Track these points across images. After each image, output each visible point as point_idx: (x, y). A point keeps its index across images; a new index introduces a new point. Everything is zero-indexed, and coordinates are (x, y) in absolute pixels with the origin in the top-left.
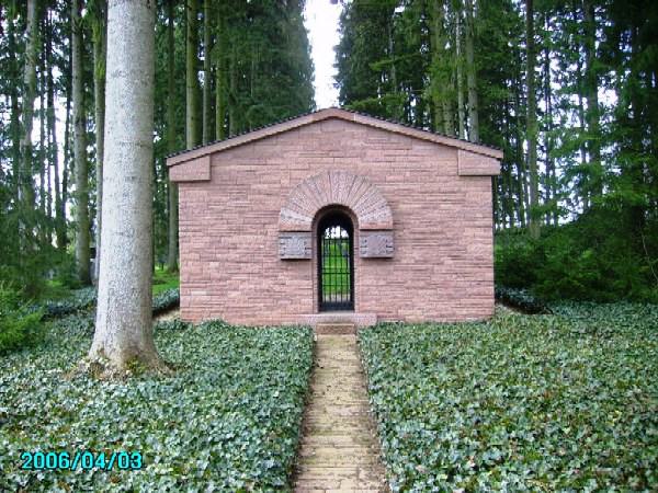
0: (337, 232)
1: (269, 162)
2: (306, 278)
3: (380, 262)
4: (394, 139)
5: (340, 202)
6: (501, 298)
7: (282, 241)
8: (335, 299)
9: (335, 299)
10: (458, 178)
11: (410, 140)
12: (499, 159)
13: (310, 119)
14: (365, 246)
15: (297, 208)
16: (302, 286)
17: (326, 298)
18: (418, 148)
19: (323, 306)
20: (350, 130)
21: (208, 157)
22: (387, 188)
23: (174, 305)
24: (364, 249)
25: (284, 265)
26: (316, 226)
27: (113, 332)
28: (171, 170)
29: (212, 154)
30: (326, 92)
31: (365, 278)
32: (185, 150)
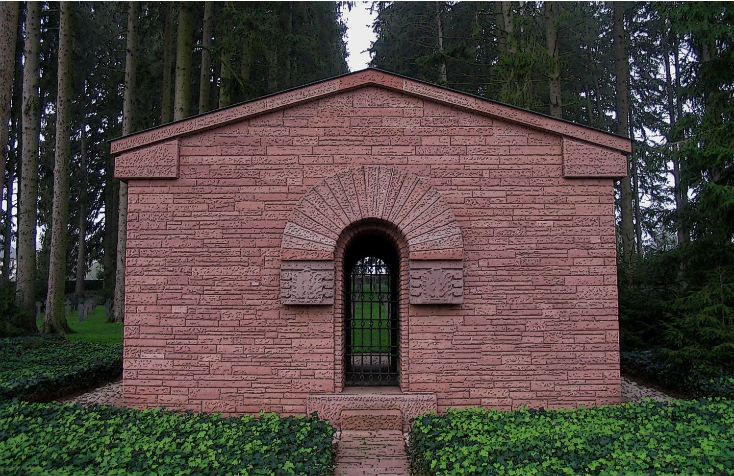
0: (377, 269)
1: (270, 151)
2: (323, 335)
3: (443, 312)
4: (465, 120)
5: (378, 216)
6: (629, 370)
7: (285, 275)
8: (372, 364)
9: (372, 364)
10: (561, 181)
11: (485, 122)
12: (624, 153)
13: (336, 85)
14: (417, 285)
15: (314, 225)
16: (319, 346)
17: (357, 360)
18: (499, 133)
19: (353, 376)
20: (398, 104)
21: (176, 142)
22: (525, 394)
23: (111, 372)
24: (417, 291)
25: (289, 314)
26: (341, 255)
27: (315, 112)
28: (118, 161)
29: (182, 137)
30: (358, 58)
31: (420, 337)
32: (171, 122)
